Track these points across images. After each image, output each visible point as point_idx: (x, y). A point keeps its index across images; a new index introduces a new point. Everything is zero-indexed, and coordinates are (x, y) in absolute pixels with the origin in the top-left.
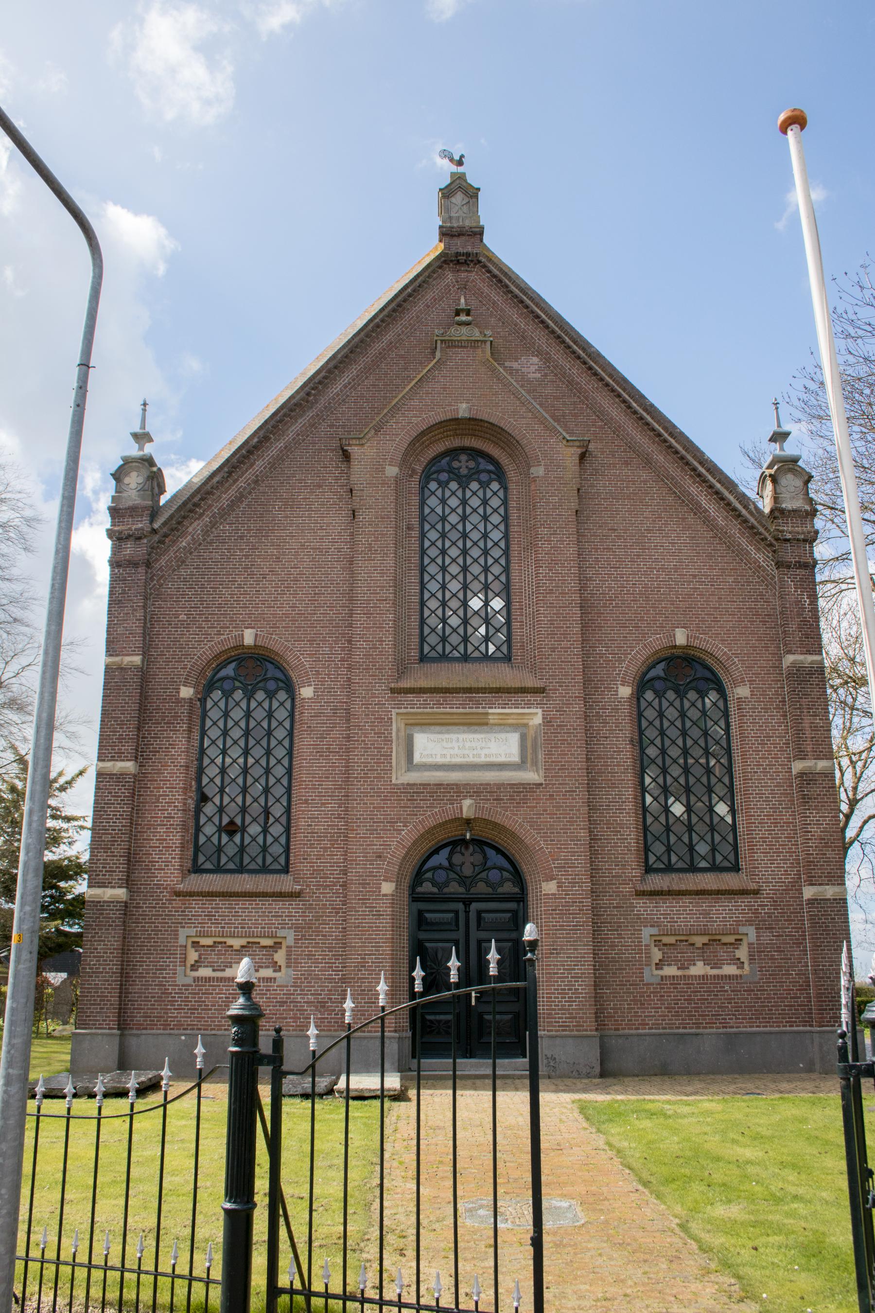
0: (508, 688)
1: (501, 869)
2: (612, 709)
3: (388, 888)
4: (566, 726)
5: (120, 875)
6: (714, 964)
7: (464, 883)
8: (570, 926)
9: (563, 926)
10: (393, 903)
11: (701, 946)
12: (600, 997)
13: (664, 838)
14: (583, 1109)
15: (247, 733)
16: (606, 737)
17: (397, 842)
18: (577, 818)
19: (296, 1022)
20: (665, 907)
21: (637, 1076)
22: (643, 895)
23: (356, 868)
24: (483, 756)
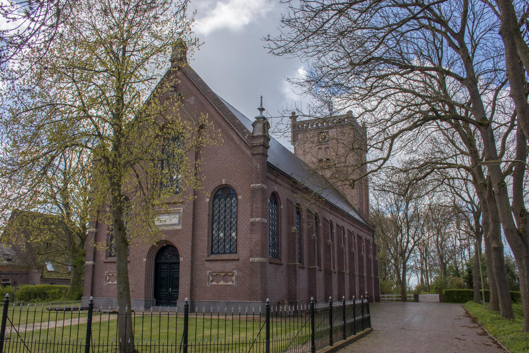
3: (145, 260)
5: (92, 258)
7: (164, 257)
20: (214, 264)
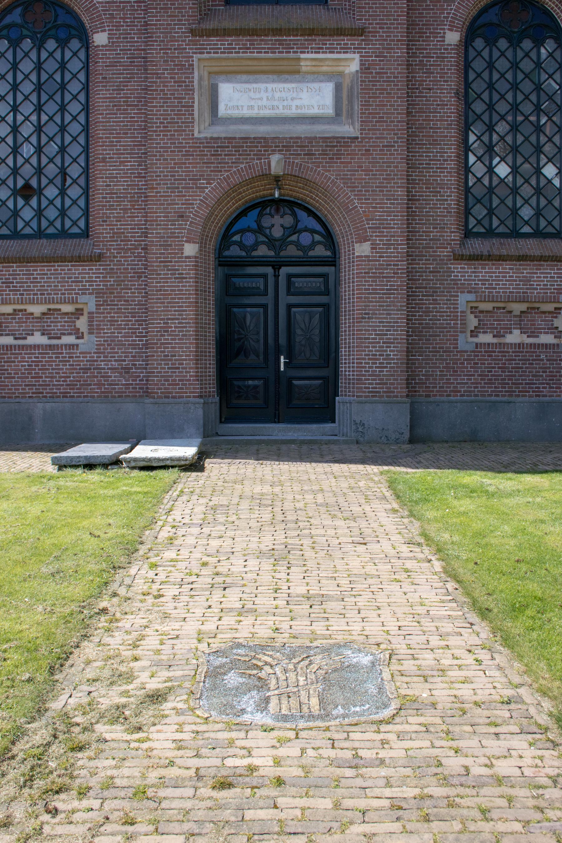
0: (322, 30)
1: (313, 232)
2: (437, 57)
4: (387, 73)
6: (532, 332)
8: (383, 290)
9: (376, 289)
10: (196, 266)
11: (519, 313)
12: (412, 364)
13: (486, 201)
14: (392, 484)
15: (39, 87)
16: (430, 89)
17: (200, 200)
18: (394, 175)
19: (101, 389)
21: (447, 442)
22: (462, 259)
23: (157, 229)
24: (294, 108)
